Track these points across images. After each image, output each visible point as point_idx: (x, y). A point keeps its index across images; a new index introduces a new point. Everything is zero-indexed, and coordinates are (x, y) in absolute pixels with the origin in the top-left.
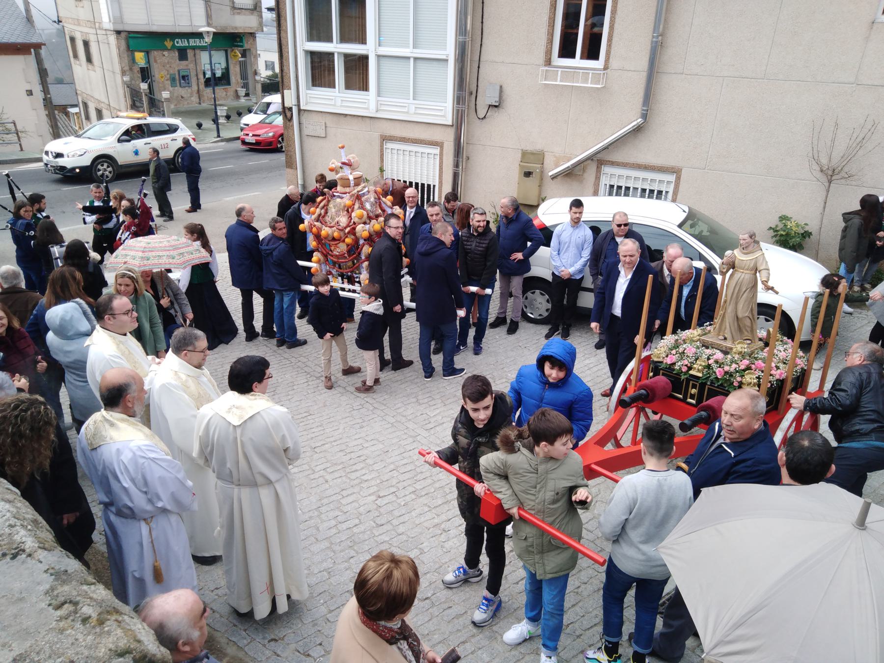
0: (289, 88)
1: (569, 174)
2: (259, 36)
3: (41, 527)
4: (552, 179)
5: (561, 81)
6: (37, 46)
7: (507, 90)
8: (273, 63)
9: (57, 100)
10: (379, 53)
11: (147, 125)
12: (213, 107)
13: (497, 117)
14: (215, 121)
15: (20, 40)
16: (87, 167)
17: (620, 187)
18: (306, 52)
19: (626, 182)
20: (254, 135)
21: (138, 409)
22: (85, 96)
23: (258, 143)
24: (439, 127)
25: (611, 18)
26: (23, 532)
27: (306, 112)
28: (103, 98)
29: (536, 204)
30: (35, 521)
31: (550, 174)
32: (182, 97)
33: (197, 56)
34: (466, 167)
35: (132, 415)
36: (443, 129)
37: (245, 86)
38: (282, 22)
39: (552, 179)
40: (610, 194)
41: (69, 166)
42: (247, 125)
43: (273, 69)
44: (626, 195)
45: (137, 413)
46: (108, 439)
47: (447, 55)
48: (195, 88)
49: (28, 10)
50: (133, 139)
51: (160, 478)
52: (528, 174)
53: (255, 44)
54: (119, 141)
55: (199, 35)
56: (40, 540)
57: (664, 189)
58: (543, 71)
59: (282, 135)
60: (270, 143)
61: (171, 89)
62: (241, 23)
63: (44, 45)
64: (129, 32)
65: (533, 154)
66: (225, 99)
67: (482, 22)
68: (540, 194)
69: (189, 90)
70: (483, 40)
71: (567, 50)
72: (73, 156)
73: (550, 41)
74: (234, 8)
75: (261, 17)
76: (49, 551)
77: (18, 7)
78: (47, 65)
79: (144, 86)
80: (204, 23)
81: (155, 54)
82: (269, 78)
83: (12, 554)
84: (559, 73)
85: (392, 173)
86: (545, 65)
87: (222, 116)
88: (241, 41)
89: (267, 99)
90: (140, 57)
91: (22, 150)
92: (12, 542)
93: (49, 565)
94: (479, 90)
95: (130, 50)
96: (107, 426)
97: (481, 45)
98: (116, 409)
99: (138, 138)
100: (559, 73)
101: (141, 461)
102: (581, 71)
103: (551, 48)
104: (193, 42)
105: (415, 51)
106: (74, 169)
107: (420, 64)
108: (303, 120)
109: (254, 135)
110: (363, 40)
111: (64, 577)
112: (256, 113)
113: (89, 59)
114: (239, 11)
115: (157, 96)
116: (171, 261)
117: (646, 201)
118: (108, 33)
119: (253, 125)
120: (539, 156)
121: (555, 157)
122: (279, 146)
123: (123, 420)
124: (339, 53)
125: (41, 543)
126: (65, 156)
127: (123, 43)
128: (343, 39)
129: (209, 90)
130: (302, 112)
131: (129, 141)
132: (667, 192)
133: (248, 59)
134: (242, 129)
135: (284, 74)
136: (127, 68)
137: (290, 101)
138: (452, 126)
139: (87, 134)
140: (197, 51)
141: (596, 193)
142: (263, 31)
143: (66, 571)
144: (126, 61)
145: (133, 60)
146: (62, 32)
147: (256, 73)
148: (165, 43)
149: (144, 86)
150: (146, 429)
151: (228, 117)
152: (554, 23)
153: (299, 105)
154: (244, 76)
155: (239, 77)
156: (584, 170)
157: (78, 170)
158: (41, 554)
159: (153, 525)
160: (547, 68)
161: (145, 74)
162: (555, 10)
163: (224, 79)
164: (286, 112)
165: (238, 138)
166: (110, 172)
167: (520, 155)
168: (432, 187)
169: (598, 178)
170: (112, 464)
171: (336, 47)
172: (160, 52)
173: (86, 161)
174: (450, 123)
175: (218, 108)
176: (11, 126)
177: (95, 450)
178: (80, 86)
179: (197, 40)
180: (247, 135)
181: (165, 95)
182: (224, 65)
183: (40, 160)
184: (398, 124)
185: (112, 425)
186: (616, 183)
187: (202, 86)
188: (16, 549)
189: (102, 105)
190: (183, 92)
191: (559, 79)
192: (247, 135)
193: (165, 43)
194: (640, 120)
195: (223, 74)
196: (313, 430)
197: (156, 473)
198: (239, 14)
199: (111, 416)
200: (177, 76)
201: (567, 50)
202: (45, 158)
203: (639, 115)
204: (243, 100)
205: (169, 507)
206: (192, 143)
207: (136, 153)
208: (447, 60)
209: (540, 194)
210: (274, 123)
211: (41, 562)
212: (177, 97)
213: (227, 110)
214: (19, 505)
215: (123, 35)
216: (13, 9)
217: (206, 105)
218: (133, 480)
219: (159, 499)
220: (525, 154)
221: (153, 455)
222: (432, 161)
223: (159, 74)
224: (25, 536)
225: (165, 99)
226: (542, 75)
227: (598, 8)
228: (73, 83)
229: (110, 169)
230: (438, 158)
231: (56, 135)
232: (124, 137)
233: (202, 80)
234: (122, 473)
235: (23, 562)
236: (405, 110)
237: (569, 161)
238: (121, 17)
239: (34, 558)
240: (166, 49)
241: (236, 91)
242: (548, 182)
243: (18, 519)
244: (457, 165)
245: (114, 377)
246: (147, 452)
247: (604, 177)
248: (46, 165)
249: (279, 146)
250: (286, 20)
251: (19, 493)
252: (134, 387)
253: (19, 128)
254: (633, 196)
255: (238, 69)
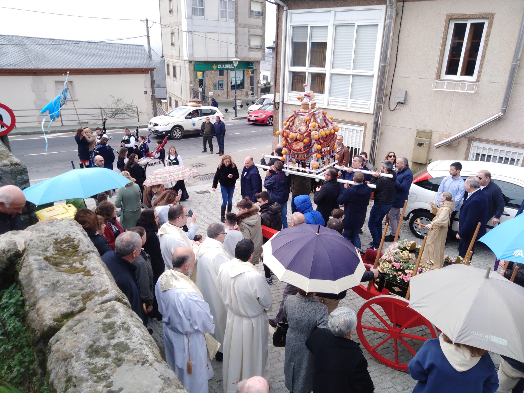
0: (279, 92)
1: (450, 146)
2: (262, 63)
3: (153, 345)
4: (437, 148)
5: (446, 88)
6: (152, 70)
7: (410, 94)
8: (267, 77)
9: (157, 97)
10: (332, 72)
11: (201, 110)
12: (235, 100)
13: (403, 111)
14: (235, 108)
15: (144, 67)
16: (169, 131)
17: (483, 155)
18: (290, 72)
19: (488, 152)
20: (255, 116)
21: (190, 271)
22: (171, 94)
23: (256, 121)
24: (365, 115)
25: (483, 51)
26: (147, 349)
27: (287, 105)
28: (179, 96)
29: (424, 163)
30: (151, 341)
31: (436, 145)
32: (219, 95)
33: (229, 74)
34: (380, 138)
35: (186, 274)
36: (368, 116)
37: (252, 89)
38: (279, 55)
39: (437, 148)
40: (477, 159)
41: (160, 131)
42: (252, 111)
43: (267, 79)
44: (488, 160)
45: (189, 273)
46: (173, 286)
47: (373, 74)
48: (226, 90)
49: (150, 52)
50: (193, 117)
51: (198, 312)
52: (420, 144)
53: (259, 67)
54: (186, 118)
55: (231, 63)
56: (155, 355)
57: (516, 158)
58: (435, 82)
59: (272, 117)
60: (263, 121)
61: (213, 91)
62: (253, 56)
63: (155, 69)
64: (196, 61)
65: (424, 132)
66: (241, 96)
67: (397, 54)
68: (428, 157)
69: (223, 91)
70: (397, 65)
71: (452, 70)
72: (163, 125)
73: (441, 65)
74: (250, 48)
75: (264, 52)
76: (160, 363)
77: (145, 50)
78: (155, 78)
79: (200, 89)
80: (234, 56)
81: (207, 72)
82: (265, 85)
83: (142, 362)
84: (467, 85)
85: (355, 144)
86: (436, 79)
87: (238, 106)
88: (252, 65)
89: (264, 97)
90: (200, 74)
91: (139, 121)
92: (142, 354)
93: (161, 373)
94: (392, 94)
95: (196, 70)
96: (173, 279)
97: (395, 67)
98: (180, 270)
99: (195, 117)
100: (467, 85)
101: (190, 301)
102: (461, 83)
103: (441, 69)
104: (227, 66)
105: (354, 71)
106: (162, 132)
107: (356, 78)
108: (285, 109)
109: (255, 116)
110: (323, 66)
111: (169, 382)
112: (257, 104)
113: (175, 76)
114: (252, 49)
115: (206, 95)
116: (178, 176)
117: (502, 165)
118: (186, 62)
119: (255, 111)
120: (429, 134)
121: (440, 134)
122: (268, 122)
123: (181, 277)
124: (309, 73)
125: (156, 357)
126: (159, 125)
127: (192, 67)
128: (312, 64)
129: (233, 92)
130: (285, 105)
131: (191, 118)
132: (518, 160)
133: (255, 75)
134: (249, 113)
135: (277, 84)
136: (193, 80)
137: (279, 99)
138: (373, 114)
139: (170, 115)
140: (229, 71)
141: (466, 158)
142: (264, 60)
143: (169, 378)
144: (193, 76)
145: (196, 76)
146: (163, 62)
147: (258, 82)
148: (213, 67)
149: (200, 89)
150: (193, 283)
151: (241, 106)
152: (444, 54)
153: (283, 101)
154: (252, 84)
155: (249, 84)
156: (459, 144)
157: (164, 133)
158: (156, 365)
159: (190, 338)
160: (437, 81)
161: (201, 83)
162: (445, 46)
163: (241, 86)
164: (276, 104)
165: (246, 118)
166: (180, 134)
167: (416, 133)
168: (358, 150)
169: (468, 149)
170: (174, 301)
171: (307, 69)
172: (210, 71)
173: (169, 128)
174: (372, 112)
175: (237, 101)
176: (135, 110)
177: (165, 292)
178: (168, 89)
179: (229, 65)
180: (251, 116)
181: (211, 94)
182: (242, 78)
183: (147, 127)
184: (340, 113)
185: (176, 279)
186: (481, 152)
187: (229, 89)
188: (144, 359)
189: (178, 99)
190: (219, 92)
191: (445, 87)
192: (251, 116)
193: (213, 67)
194: (501, 113)
195: (241, 83)
196: (279, 291)
197: (196, 309)
198: (252, 51)
199: (176, 273)
200: (217, 84)
201: (452, 70)
202: (149, 126)
203: (500, 110)
204: (250, 97)
205: (200, 330)
206: (222, 119)
207: (194, 125)
208: (373, 76)
209: (428, 157)
210: (266, 110)
211: (156, 370)
212: (216, 95)
213: (242, 102)
214: (143, 330)
215: (193, 63)
216: (143, 51)
217: (230, 99)
218: (184, 312)
219: (196, 324)
220: (419, 132)
221: (196, 299)
222: (359, 134)
223: (208, 83)
224: (148, 351)
225: (211, 96)
226: (434, 85)
227: (1, 35)
228: (165, 87)
229: (180, 133)
230: (363, 132)
231: (155, 115)
232: (189, 116)
233: (230, 86)
234: (179, 307)
235: (148, 368)
236: (345, 104)
237: (449, 137)
238: (193, 54)
239: (153, 366)
240: (213, 70)
241: (247, 92)
242: (433, 149)
243: (144, 340)
244: (375, 137)
245: (180, 251)
246: (193, 297)
247: (473, 148)
248: (150, 129)
249: (268, 122)
250: (281, 55)
251: (142, 322)
252: (190, 259)
253: (139, 110)
254: (493, 161)
255: (249, 80)
